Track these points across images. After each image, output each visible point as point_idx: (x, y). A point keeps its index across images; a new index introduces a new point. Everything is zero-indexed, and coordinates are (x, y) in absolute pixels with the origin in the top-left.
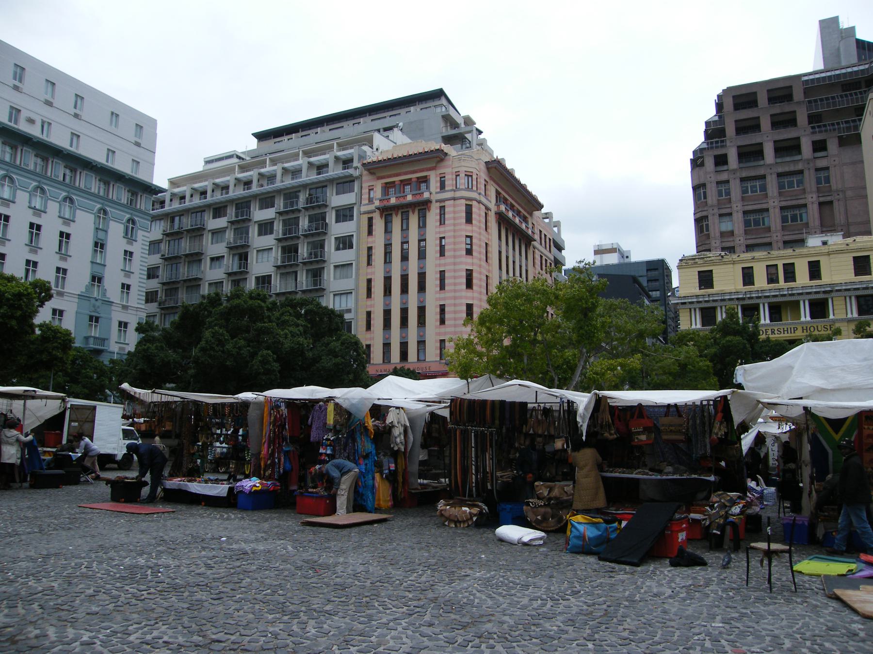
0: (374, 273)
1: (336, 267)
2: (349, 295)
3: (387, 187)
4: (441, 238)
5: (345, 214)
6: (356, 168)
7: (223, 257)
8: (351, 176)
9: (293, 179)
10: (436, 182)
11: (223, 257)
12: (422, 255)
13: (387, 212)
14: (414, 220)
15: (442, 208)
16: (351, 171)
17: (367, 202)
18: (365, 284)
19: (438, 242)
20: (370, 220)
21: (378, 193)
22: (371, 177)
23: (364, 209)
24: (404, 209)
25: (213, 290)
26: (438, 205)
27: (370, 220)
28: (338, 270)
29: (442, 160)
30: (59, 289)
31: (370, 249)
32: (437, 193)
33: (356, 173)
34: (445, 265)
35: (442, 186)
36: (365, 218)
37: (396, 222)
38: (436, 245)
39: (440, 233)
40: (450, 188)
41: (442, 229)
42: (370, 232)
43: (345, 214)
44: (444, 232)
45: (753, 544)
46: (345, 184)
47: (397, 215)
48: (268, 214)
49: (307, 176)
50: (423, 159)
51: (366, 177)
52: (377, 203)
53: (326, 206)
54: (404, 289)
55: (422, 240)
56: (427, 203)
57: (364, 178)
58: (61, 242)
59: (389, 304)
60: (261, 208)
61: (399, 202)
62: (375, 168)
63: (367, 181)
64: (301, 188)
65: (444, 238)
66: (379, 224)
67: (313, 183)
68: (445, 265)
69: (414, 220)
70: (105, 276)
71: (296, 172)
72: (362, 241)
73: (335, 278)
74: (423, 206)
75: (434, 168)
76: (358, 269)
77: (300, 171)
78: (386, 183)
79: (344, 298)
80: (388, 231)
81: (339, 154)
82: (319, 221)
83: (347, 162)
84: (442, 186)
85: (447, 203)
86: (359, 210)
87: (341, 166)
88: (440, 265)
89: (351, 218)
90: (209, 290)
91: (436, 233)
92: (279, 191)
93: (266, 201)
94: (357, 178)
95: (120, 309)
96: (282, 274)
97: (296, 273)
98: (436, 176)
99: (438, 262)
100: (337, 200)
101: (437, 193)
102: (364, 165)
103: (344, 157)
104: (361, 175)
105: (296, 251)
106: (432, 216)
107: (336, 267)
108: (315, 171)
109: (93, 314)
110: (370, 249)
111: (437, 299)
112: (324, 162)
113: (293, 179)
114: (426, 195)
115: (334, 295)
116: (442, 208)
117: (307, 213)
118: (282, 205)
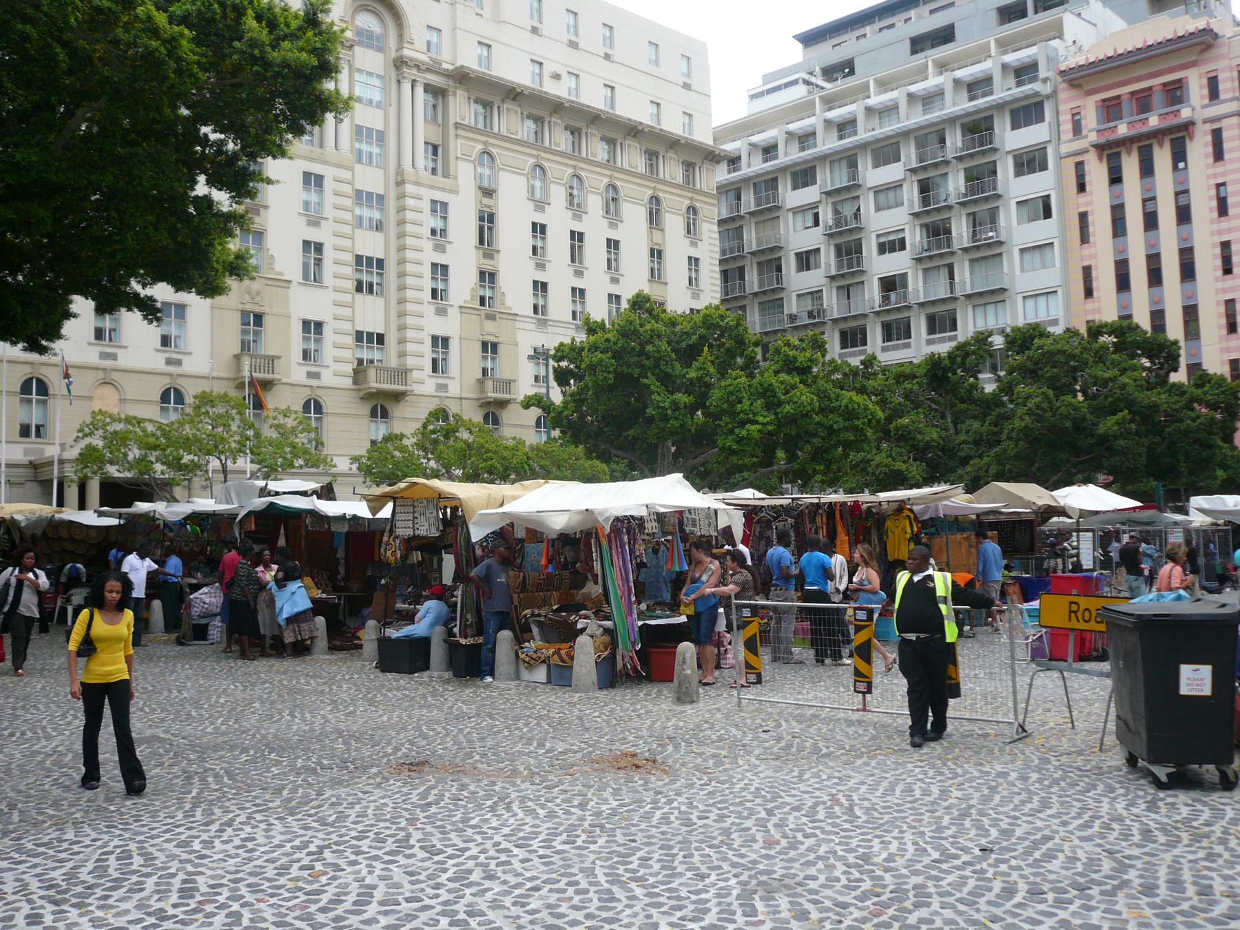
0: (1094, 256)
1: (1022, 251)
2: (1051, 297)
3: (1111, 109)
4: (1218, 186)
5: (1030, 162)
6: (1045, 80)
7: (818, 250)
8: (1037, 94)
9: (925, 112)
10: (1201, 87)
11: (818, 250)
12: (1184, 215)
13: (1111, 151)
14: (1162, 157)
15: (1217, 136)
16: (1036, 87)
17: (1070, 136)
18: (1079, 276)
19: (1213, 192)
20: (1080, 166)
21: (1090, 119)
22: (1072, 93)
23: (1065, 149)
24: (1144, 145)
25: (808, 305)
26: (1209, 127)
27: (1080, 166)
28: (1027, 256)
29: (1209, 47)
30: (540, 316)
31: (1083, 217)
32: (1203, 107)
33: (1046, 89)
34: (1229, 231)
35: (1214, 94)
36: (1070, 164)
37: (1130, 165)
38: (1210, 198)
39: (1215, 176)
40: (1230, 95)
41: (1220, 168)
42: (1082, 187)
43: (1030, 162)
44: (1224, 174)
45: (135, 286)
46: (1027, 112)
47: (1161, 145)
48: (893, 172)
49: (786, 155)
50: (1167, 53)
51: (1064, 94)
52: (1093, 137)
53: (995, 150)
54: (1155, 277)
55: (1182, 193)
56: (1187, 127)
57: (1062, 95)
58: (572, 247)
59: (1160, 301)
60: (877, 165)
61: (1133, 132)
62: (1079, 78)
63: (1068, 101)
64: (946, 126)
65: (1224, 184)
66: (1097, 173)
67: (836, 153)
68: (1229, 231)
69: (1162, 157)
70: (93, 312)
71: (929, 99)
72: (1067, 204)
73: (1022, 270)
74: (1178, 138)
75: (1193, 64)
76: (1065, 251)
77: (775, 146)
78: (1104, 100)
79: (1042, 301)
80: (1116, 179)
81: (831, 115)
82: (981, 179)
83: (1025, 72)
84: (1214, 94)
85: (1225, 123)
86: (1057, 150)
87: (965, 94)
88: (1220, 232)
89: (1044, 167)
90: (798, 307)
91: (1208, 177)
92: (906, 134)
93: (885, 151)
94: (1048, 97)
95: (533, 327)
96: (926, 271)
97: (951, 268)
98: (1200, 76)
99: (1215, 227)
100: (1012, 139)
101: (1203, 107)
102: (1062, 73)
103: (763, 144)
104: (1055, 92)
105: (948, 232)
106: (1199, 149)
107: (1022, 251)
108: (835, 134)
109: (248, 307)
110: (1083, 217)
111: (1218, 291)
112: (810, 129)
113: (925, 112)
114: (1185, 113)
115: (1024, 298)
116: (1217, 136)
117: (961, 166)
118: (913, 156)
